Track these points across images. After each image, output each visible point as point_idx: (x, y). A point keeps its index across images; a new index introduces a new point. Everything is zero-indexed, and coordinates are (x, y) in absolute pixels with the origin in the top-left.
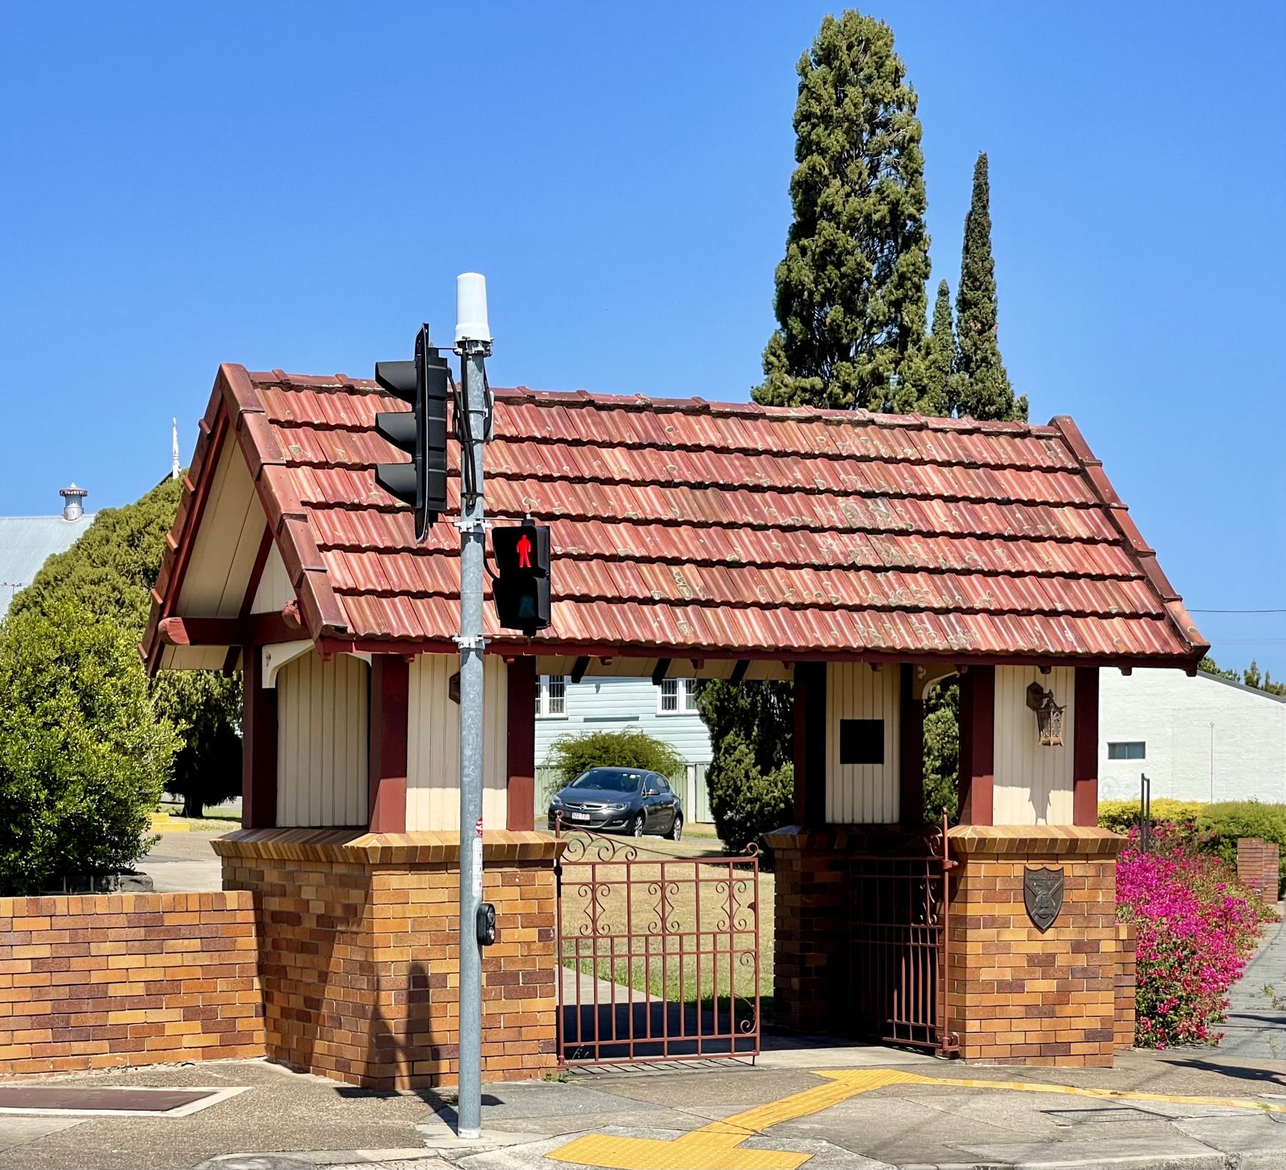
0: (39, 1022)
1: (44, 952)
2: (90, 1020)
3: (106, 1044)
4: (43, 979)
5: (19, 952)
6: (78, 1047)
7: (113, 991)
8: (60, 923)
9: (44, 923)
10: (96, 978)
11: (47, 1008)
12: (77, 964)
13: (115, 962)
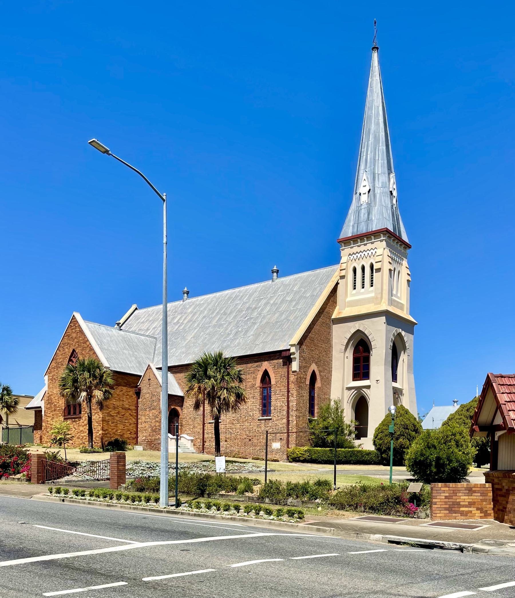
0: (446, 509)
1: (447, 495)
2: (457, 509)
3: (460, 515)
4: (447, 500)
5: (442, 494)
6: (454, 515)
7: (461, 503)
8: (451, 489)
9: (447, 489)
10: (458, 501)
11: (448, 506)
12: (454, 497)
13: (462, 497)
